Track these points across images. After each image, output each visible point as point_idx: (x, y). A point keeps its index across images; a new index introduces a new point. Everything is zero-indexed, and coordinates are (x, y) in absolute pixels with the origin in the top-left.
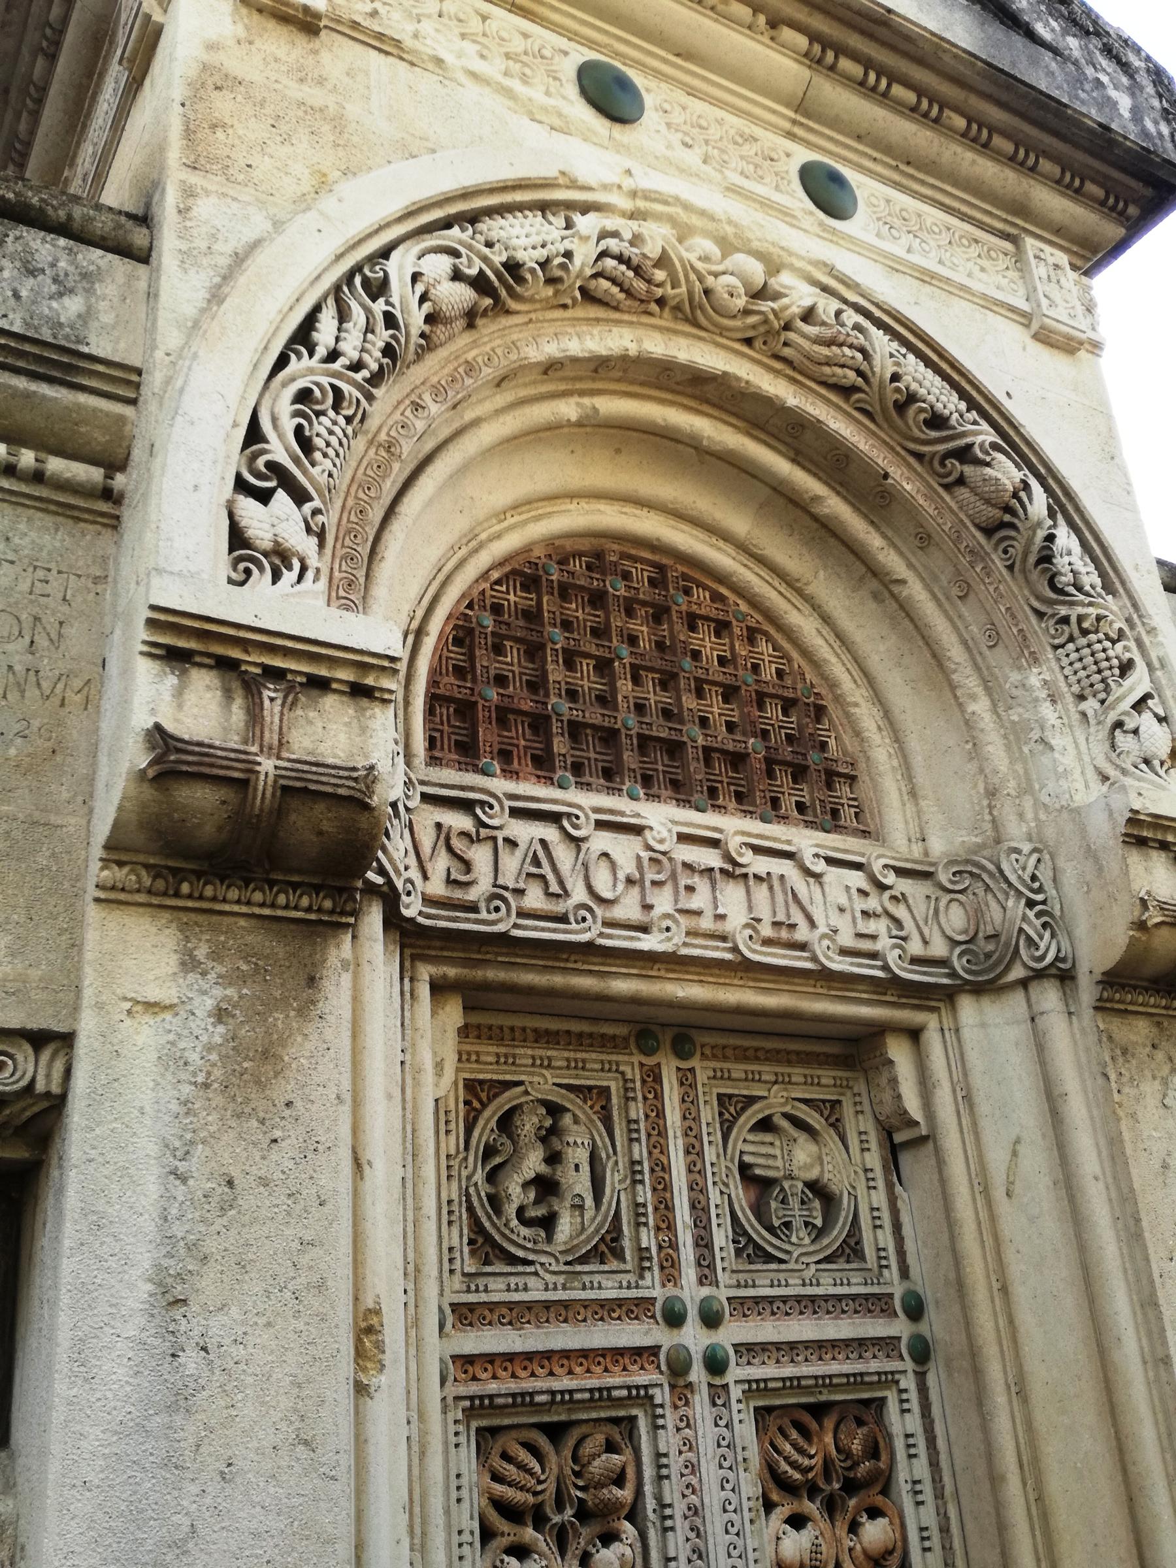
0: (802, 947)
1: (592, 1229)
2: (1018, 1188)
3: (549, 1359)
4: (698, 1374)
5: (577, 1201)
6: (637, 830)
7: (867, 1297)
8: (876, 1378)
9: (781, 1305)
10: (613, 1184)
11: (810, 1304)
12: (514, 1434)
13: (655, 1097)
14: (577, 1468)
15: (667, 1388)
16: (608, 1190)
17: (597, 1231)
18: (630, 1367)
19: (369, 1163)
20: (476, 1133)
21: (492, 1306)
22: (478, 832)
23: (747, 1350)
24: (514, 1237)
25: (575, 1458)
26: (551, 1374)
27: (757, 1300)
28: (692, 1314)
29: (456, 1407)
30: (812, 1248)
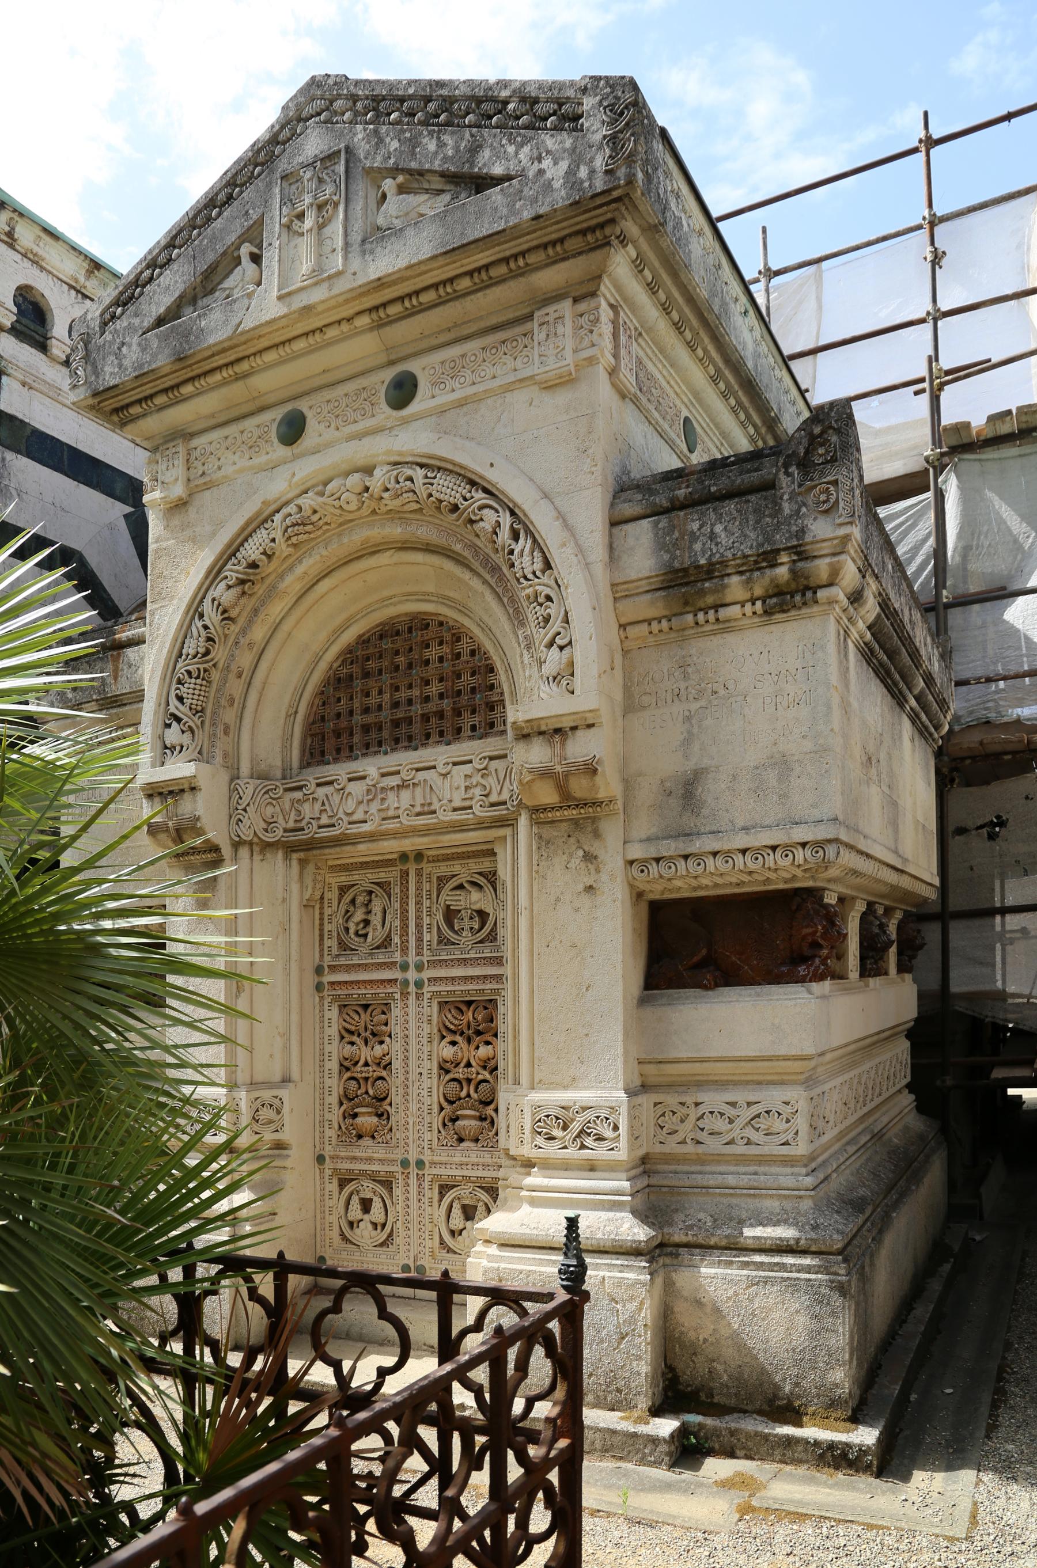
0: (434, 812)
4: (412, 988)
23: (432, 980)
27: (440, 961)
28: (412, 966)
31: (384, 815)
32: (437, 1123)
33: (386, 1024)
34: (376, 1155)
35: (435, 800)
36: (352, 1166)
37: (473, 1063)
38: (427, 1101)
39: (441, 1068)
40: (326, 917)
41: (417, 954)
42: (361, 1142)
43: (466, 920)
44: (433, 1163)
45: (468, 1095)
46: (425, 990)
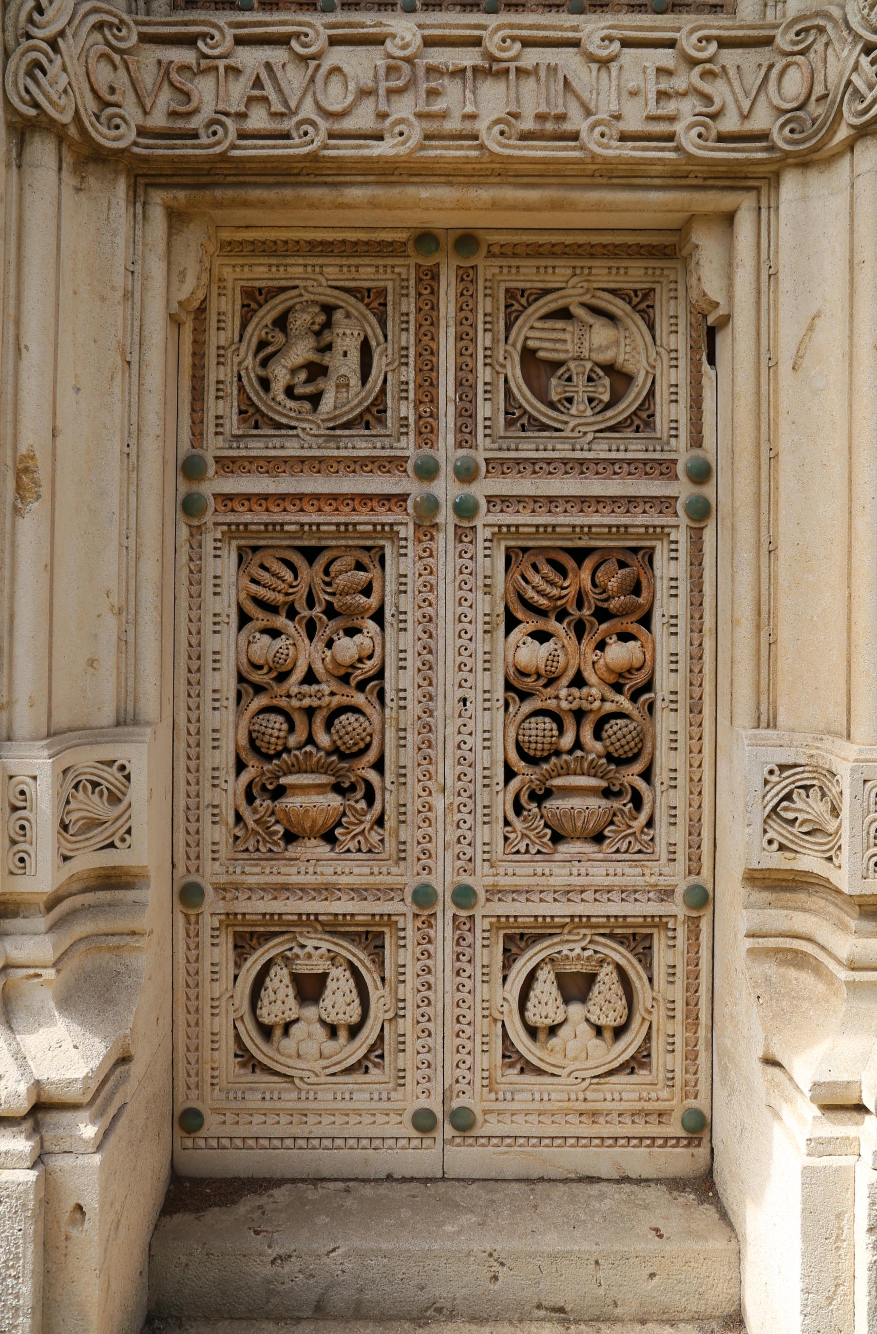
0: (575, 136)
1: (356, 402)
2: (806, 362)
3: (301, 499)
4: (446, 517)
5: (342, 381)
6: (378, 41)
7: (645, 462)
8: (642, 530)
9: (544, 466)
10: (380, 366)
11: (581, 466)
12: (270, 551)
13: (432, 293)
14: (327, 579)
15: (411, 526)
16: (374, 371)
17: (360, 403)
18: (378, 509)
19: (26, 347)
20: (250, 329)
21: (251, 459)
22: (199, 64)
24: (280, 409)
25: (326, 572)
26: (302, 510)
27: (518, 461)
29: (216, 530)
30: (593, 419)
31: (432, 126)
32: (503, 804)
33: (367, 591)
34: (344, 880)
35: (574, 111)
36: (277, 906)
37: (589, 675)
38: (483, 758)
39: (509, 686)
40: (212, 352)
41: (459, 445)
42: (294, 850)
43: (580, 381)
44: (495, 892)
45: (578, 744)
46: (479, 522)
